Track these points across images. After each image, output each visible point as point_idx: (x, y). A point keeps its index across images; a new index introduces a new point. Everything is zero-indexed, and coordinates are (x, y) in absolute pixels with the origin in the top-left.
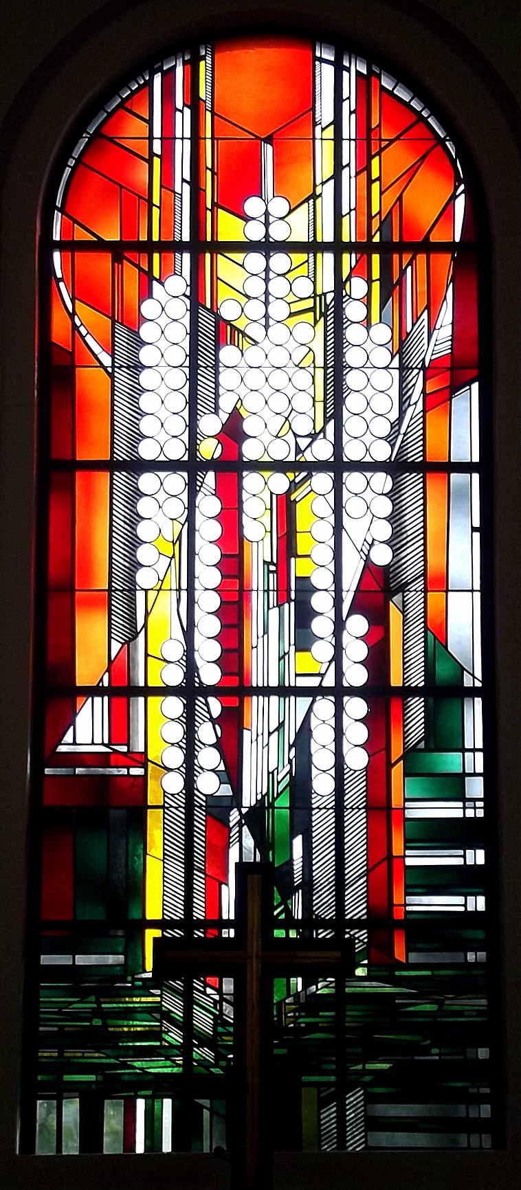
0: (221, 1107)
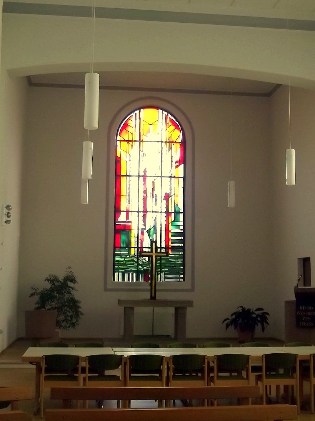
0: (143, 275)
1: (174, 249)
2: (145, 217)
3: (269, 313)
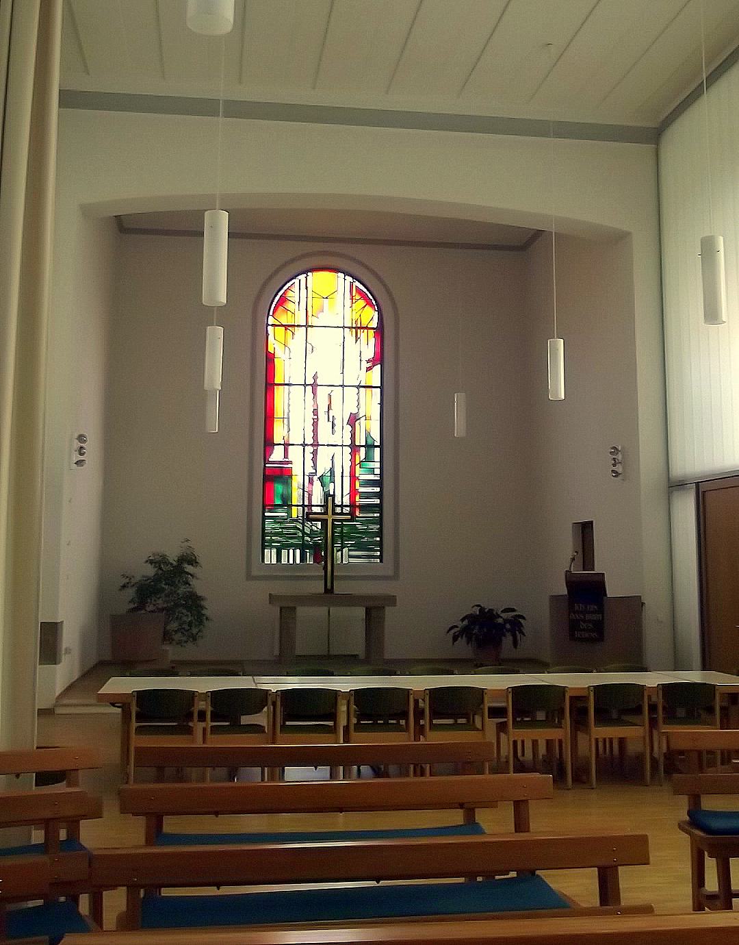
1: (364, 508)
2: (315, 453)
3: (524, 616)
